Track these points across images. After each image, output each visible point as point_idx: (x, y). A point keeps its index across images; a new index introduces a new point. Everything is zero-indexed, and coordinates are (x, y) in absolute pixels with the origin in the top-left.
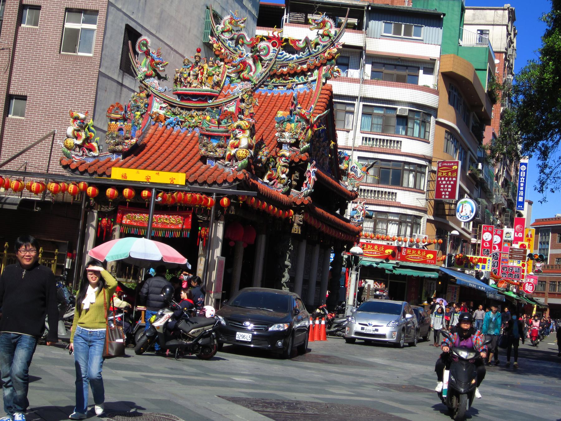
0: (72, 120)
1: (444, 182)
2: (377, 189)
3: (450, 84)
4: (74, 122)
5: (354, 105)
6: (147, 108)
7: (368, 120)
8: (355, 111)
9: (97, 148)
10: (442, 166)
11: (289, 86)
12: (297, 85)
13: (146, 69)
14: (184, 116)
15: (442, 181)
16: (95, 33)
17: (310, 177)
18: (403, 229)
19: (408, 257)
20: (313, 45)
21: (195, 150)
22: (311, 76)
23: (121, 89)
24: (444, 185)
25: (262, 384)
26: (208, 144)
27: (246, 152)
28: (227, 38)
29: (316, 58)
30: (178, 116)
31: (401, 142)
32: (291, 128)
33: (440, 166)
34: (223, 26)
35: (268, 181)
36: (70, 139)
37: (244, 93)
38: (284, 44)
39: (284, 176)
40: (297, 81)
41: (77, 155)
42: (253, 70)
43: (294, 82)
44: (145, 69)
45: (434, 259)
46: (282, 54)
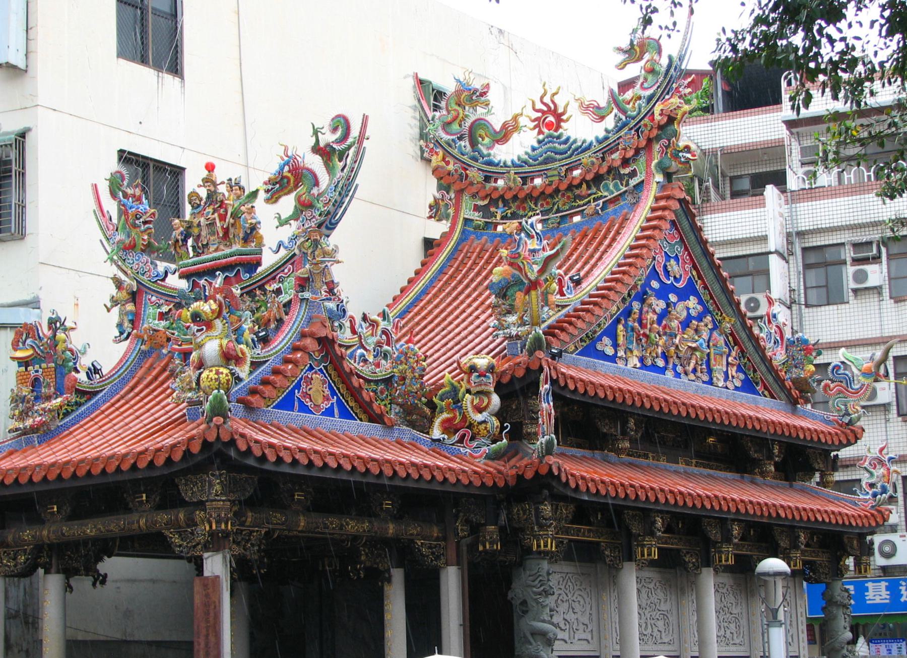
22: (633, 174)
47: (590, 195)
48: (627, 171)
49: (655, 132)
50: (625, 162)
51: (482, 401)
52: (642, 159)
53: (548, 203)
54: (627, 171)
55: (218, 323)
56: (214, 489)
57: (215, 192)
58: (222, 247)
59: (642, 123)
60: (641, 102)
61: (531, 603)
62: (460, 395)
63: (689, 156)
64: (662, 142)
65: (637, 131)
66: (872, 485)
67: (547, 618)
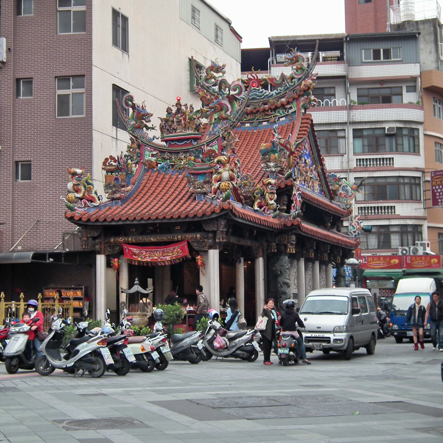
0: (70, 176)
1: (439, 190)
2: (376, 205)
3: (434, 98)
4: (72, 178)
5: (344, 130)
6: (139, 157)
7: (359, 142)
8: (346, 136)
9: (97, 199)
10: (435, 176)
11: (272, 120)
12: (279, 118)
13: (134, 122)
14: (173, 160)
15: (437, 190)
16: (85, 95)
17: (296, 200)
18: (405, 237)
19: (413, 264)
20: (289, 80)
21: (186, 189)
22: (291, 108)
23: (117, 144)
24: (439, 193)
25: (238, 386)
26: (195, 181)
27: (229, 184)
28: (211, 85)
29: (294, 91)
30: (168, 161)
31: (393, 158)
32: (275, 158)
33: (433, 175)
34: (206, 75)
35: (258, 209)
36: (71, 194)
37: (223, 131)
38: (263, 82)
39: (272, 202)
40: (279, 115)
41: (79, 207)
42: (230, 110)
43: (277, 116)
44: (133, 122)
45: (439, 262)
46: (262, 92)
47: (271, 115)
48: (289, 106)
49: (302, 93)
50: (288, 103)
51: (272, 196)
52: (295, 103)
53: (253, 116)
54: (289, 106)
55: (228, 165)
56: (222, 225)
57: (181, 109)
58: (183, 131)
59: (296, 88)
60: (295, 80)
61: (283, 272)
62: (265, 193)
63: (315, 103)
64: (305, 96)
65: (294, 91)
66: (354, 232)
67: (287, 277)
